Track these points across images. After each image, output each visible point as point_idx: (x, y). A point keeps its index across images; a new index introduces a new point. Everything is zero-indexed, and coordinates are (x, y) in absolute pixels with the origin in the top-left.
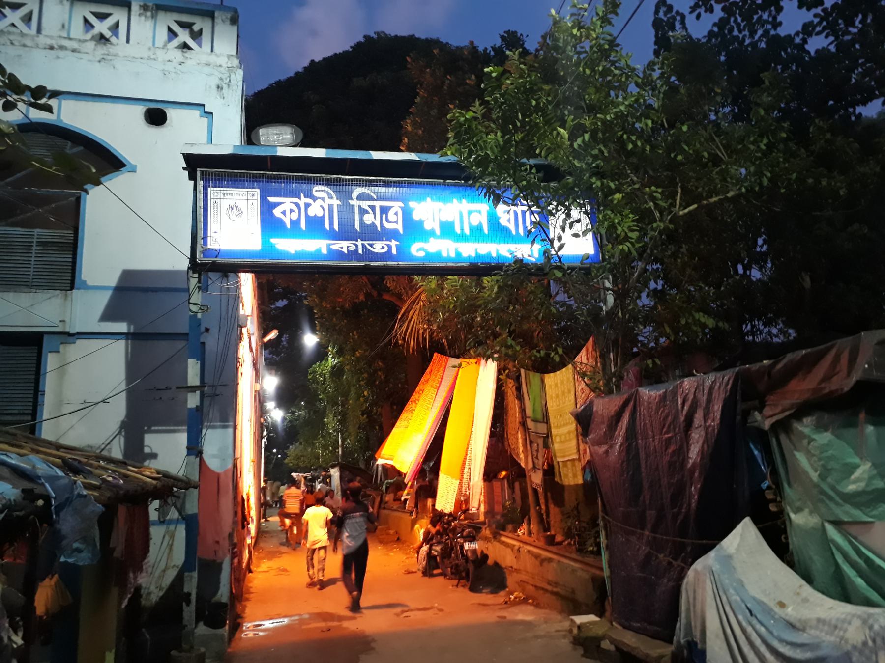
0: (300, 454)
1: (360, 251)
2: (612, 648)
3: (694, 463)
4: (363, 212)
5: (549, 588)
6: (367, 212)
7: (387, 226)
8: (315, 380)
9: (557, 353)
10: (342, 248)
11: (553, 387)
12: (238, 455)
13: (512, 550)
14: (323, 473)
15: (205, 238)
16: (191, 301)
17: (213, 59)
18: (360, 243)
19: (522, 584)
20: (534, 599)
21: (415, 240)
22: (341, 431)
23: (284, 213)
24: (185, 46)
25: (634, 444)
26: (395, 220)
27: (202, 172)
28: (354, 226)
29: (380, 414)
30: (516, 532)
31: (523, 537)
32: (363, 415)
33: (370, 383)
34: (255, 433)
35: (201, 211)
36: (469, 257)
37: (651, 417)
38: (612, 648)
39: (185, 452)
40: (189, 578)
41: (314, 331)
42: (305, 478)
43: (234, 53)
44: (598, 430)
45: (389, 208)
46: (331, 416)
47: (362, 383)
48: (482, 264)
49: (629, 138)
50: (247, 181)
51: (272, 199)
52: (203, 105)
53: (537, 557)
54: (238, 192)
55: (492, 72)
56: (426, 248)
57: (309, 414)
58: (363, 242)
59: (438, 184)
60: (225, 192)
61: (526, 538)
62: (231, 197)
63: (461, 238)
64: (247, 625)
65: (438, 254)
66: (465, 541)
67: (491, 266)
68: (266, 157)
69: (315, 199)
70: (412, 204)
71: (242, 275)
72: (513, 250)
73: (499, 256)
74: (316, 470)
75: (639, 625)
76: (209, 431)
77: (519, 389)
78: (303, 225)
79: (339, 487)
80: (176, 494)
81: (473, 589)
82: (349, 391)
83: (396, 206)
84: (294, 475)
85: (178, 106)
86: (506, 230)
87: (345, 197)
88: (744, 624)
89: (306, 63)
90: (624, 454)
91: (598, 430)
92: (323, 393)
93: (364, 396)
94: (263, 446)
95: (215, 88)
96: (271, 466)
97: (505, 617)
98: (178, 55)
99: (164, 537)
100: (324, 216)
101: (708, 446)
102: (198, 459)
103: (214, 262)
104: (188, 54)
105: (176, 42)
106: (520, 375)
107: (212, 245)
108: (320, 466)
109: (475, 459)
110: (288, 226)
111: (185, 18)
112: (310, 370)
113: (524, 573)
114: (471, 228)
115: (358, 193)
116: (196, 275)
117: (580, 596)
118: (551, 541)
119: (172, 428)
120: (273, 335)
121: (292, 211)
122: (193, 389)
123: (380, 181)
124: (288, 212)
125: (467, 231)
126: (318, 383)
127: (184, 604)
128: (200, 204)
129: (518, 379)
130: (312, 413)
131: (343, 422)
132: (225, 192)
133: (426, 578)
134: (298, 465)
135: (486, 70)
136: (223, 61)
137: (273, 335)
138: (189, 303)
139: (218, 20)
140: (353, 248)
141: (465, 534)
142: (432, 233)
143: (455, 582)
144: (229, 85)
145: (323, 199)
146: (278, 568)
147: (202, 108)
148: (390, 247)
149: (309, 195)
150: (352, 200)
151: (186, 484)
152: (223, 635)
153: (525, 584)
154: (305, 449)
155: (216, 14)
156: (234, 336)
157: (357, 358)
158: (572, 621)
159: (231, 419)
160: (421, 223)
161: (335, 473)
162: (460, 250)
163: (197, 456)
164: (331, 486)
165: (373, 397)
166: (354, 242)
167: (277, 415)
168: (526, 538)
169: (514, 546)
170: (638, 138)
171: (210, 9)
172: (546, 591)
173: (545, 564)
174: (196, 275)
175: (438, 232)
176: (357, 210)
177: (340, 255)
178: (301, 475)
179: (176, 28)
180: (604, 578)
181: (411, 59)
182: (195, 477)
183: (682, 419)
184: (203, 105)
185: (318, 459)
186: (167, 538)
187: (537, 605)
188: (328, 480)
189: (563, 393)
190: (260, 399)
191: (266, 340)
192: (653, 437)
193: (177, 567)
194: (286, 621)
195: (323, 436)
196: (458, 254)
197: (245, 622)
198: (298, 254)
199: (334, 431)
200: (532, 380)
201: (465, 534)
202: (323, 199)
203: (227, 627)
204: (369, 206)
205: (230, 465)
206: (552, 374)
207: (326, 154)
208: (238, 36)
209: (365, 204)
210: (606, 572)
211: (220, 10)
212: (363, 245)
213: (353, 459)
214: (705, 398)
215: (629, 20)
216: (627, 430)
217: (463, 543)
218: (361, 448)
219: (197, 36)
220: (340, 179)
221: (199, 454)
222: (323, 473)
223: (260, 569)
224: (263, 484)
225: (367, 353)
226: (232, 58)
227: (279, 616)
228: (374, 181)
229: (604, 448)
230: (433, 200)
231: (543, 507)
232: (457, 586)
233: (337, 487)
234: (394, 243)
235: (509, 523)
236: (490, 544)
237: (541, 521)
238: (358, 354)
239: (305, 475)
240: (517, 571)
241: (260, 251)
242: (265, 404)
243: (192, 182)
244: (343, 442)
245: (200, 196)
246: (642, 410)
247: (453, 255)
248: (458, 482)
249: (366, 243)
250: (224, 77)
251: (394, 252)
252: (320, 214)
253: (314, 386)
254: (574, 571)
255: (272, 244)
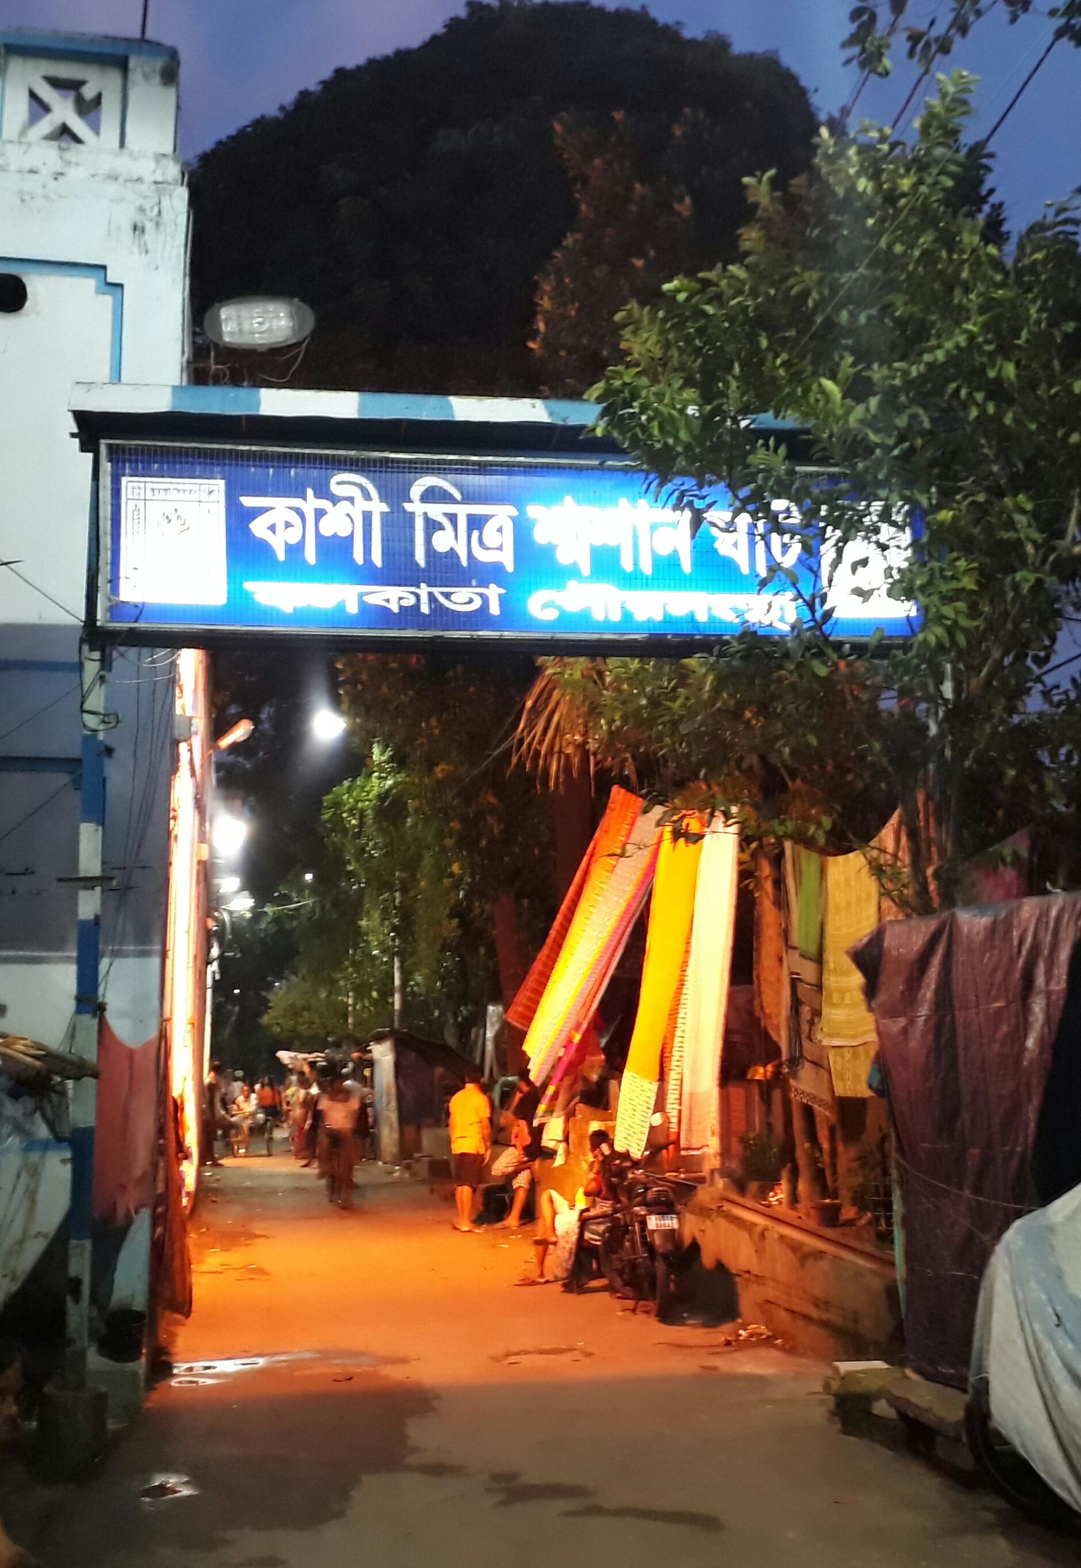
0: (301, 1002)
1: (425, 609)
2: (891, 1413)
3: (1031, 1062)
4: (432, 526)
5: (814, 1313)
6: (441, 527)
7: (481, 555)
8: (338, 824)
9: (819, 825)
10: (388, 601)
11: (842, 886)
12: (167, 1015)
13: (751, 1234)
14: (355, 1055)
15: (114, 581)
16: (86, 707)
17: (123, 164)
18: (424, 590)
19: (767, 1305)
20: (783, 1335)
21: (538, 585)
22: (402, 954)
23: (272, 528)
24: (64, 132)
25: (948, 1018)
26: (497, 545)
27: (110, 447)
28: (412, 554)
29: (490, 919)
30: (765, 1198)
31: (778, 1208)
32: (451, 916)
33: (467, 841)
34: (195, 957)
35: (106, 525)
36: (648, 621)
37: (973, 968)
38: (891, 1413)
39: (72, 1005)
40: (77, 1251)
41: (336, 703)
42: (312, 1064)
43: (168, 148)
44: (892, 987)
45: (486, 518)
46: (376, 915)
47: (449, 842)
48: (675, 635)
49: (970, 395)
50: (200, 463)
51: (248, 501)
52: (104, 268)
53: (795, 1247)
54: (180, 487)
55: (678, 291)
56: (559, 602)
57: (323, 908)
58: (431, 589)
59: (588, 468)
60: (155, 486)
61: (784, 1211)
62: (168, 497)
63: (633, 580)
64: (180, 1368)
65: (584, 616)
66: (651, 1213)
67: (693, 640)
68: (239, 417)
69: (335, 500)
70: (533, 511)
71: (184, 652)
72: (742, 607)
73: (712, 620)
74: (337, 1045)
75: (952, 1371)
76: (118, 962)
77: (779, 883)
78: (310, 554)
79: (393, 1091)
80: (58, 1088)
81: (667, 1315)
82: (419, 858)
83: (501, 515)
84: (284, 1056)
85: (51, 269)
86: (728, 566)
87: (395, 496)
88: (1041, 1336)
89: (327, 73)
90: (931, 1037)
91: (892, 987)
92: (357, 861)
93: (452, 875)
94: (209, 982)
95: (127, 229)
96: (227, 1031)
97: (715, 1368)
98: (48, 155)
99: (18, 1176)
100: (351, 537)
101: (1049, 1028)
102: (96, 1021)
103: (132, 630)
104: (75, 152)
105: (47, 125)
106: (781, 855)
107: (128, 593)
108: (349, 1037)
109: (697, 1038)
110: (281, 556)
111: (66, 71)
112: (327, 799)
113: (771, 1284)
114: (656, 560)
115: (423, 489)
116: (96, 655)
117: (866, 1328)
118: (830, 1217)
119: (36, 954)
120: (241, 732)
121: (288, 525)
122: (89, 882)
123: (468, 463)
124: (280, 528)
125: (647, 568)
126: (345, 831)
127: (69, 1298)
128: (105, 511)
129: (778, 860)
130: (328, 906)
131: (404, 930)
132: (155, 486)
133: (573, 1297)
134: (294, 1030)
135: (666, 287)
136: (147, 169)
137: (241, 732)
138: (83, 711)
139: (135, 76)
140: (411, 601)
141: (650, 1195)
142: (572, 571)
143: (630, 1303)
144: (157, 225)
145: (351, 500)
146: (245, 1267)
147: (102, 272)
148: (485, 599)
149: (324, 492)
150: (410, 501)
151: (79, 1070)
152: (135, 1374)
153: (773, 1307)
154: (315, 992)
155: (132, 63)
156: (166, 764)
157: (438, 781)
158: (836, 1369)
159: (157, 939)
160: (549, 551)
161: (383, 1054)
162: (630, 607)
163: (94, 1016)
164: (372, 1087)
165: (472, 876)
166: (412, 589)
167: (242, 904)
168: (784, 1211)
169: (754, 1225)
170: (989, 396)
171: (120, 50)
172: (806, 1317)
173: (810, 1263)
174: (96, 655)
175: (586, 569)
176: (419, 524)
177: (383, 614)
178: (301, 1056)
179: (47, 93)
180: (895, 1281)
181: (564, 125)
182: (91, 1055)
183: (1018, 975)
184: (104, 268)
185: (345, 1017)
186: (24, 1176)
187: (791, 1350)
188: (367, 1072)
189: (859, 900)
190: (206, 872)
191: (225, 742)
192: (977, 1006)
193: (45, 1236)
194: (261, 1362)
195: (356, 965)
196: (627, 616)
197: (177, 1361)
198: (299, 615)
199: (384, 951)
200: (804, 867)
201: (650, 1195)
202: (351, 500)
203: (143, 1360)
204: (446, 515)
205: (153, 1033)
206: (841, 858)
207: (359, 411)
208: (178, 108)
209: (436, 511)
210: (900, 1271)
211: (140, 52)
212: (430, 594)
213: (430, 1022)
214: (1049, 938)
215: (1017, 97)
216: (937, 991)
217: (644, 1216)
218: (449, 996)
219: (88, 108)
220: (387, 459)
221: (99, 1010)
222: (355, 1055)
223: (204, 1268)
224: (208, 1078)
225: (462, 771)
226: (164, 161)
227: (246, 1353)
228: (456, 462)
229: (902, 1022)
230: (578, 502)
231: (825, 1145)
232: (634, 1311)
233: (389, 1088)
234: (493, 592)
235: (752, 1179)
236: (708, 1222)
237: (819, 1176)
238: (439, 771)
239: (311, 1057)
240: (759, 1279)
241: (224, 607)
242: (216, 881)
243: (90, 455)
244: (406, 977)
245: (105, 495)
246: (960, 957)
247: (615, 616)
248: (655, 1087)
249: (436, 591)
250: (147, 205)
251: (495, 609)
252: (344, 532)
253: (336, 838)
254: (859, 1274)
255: (246, 591)
